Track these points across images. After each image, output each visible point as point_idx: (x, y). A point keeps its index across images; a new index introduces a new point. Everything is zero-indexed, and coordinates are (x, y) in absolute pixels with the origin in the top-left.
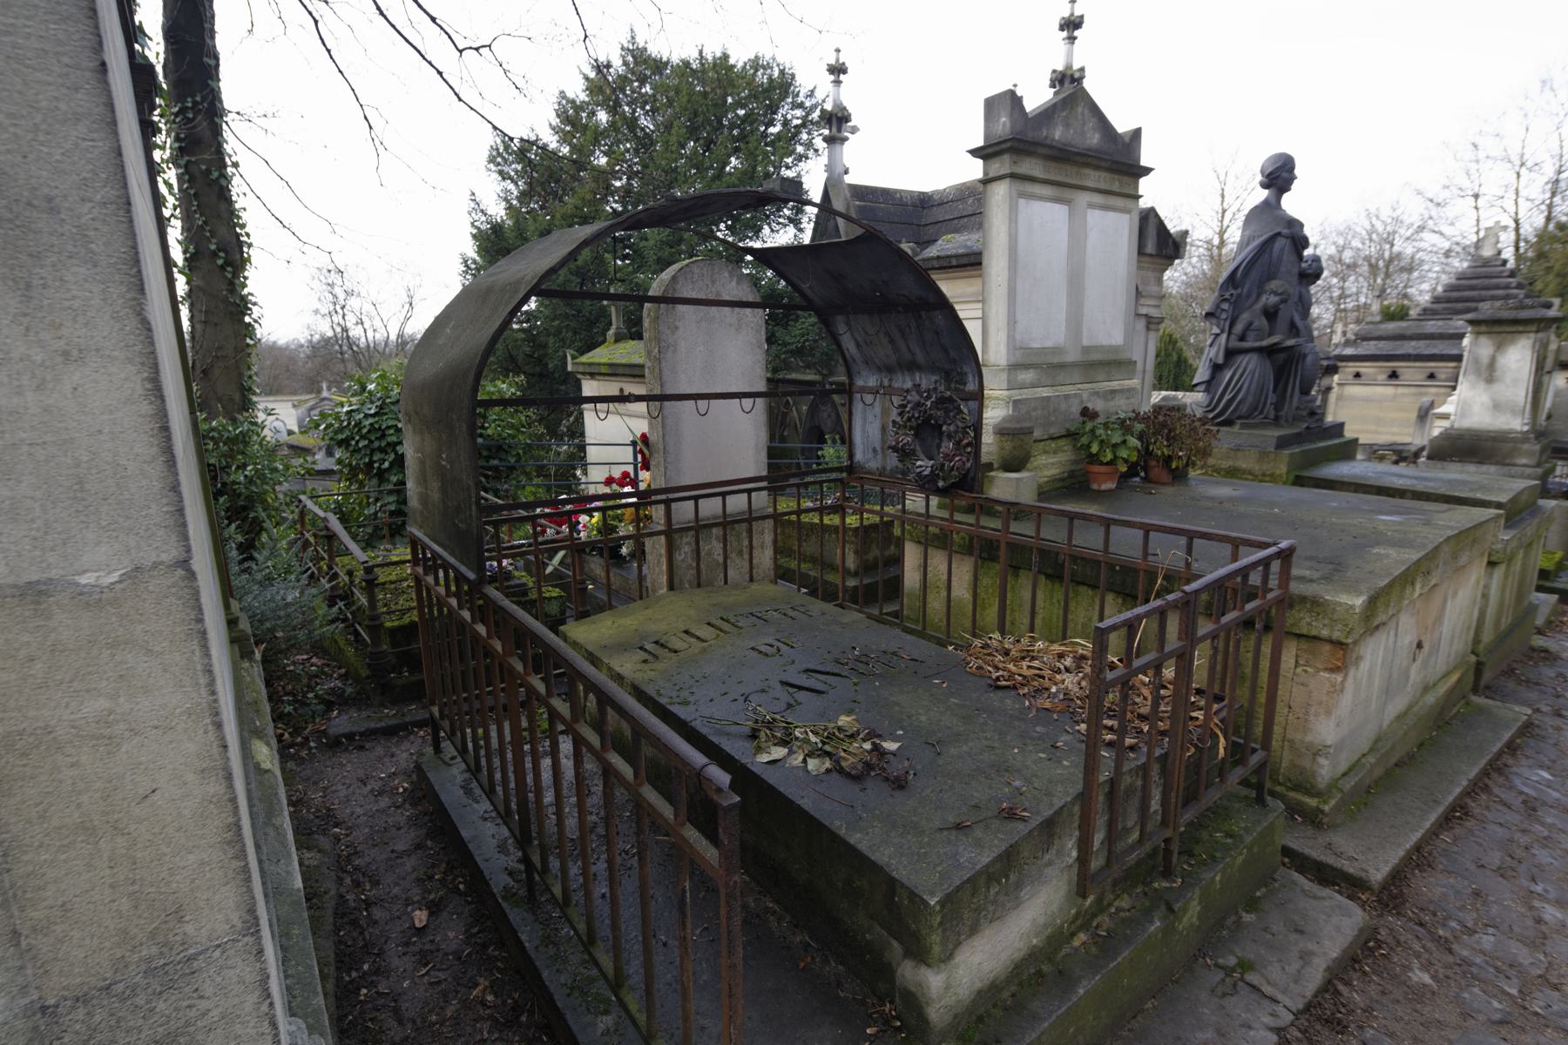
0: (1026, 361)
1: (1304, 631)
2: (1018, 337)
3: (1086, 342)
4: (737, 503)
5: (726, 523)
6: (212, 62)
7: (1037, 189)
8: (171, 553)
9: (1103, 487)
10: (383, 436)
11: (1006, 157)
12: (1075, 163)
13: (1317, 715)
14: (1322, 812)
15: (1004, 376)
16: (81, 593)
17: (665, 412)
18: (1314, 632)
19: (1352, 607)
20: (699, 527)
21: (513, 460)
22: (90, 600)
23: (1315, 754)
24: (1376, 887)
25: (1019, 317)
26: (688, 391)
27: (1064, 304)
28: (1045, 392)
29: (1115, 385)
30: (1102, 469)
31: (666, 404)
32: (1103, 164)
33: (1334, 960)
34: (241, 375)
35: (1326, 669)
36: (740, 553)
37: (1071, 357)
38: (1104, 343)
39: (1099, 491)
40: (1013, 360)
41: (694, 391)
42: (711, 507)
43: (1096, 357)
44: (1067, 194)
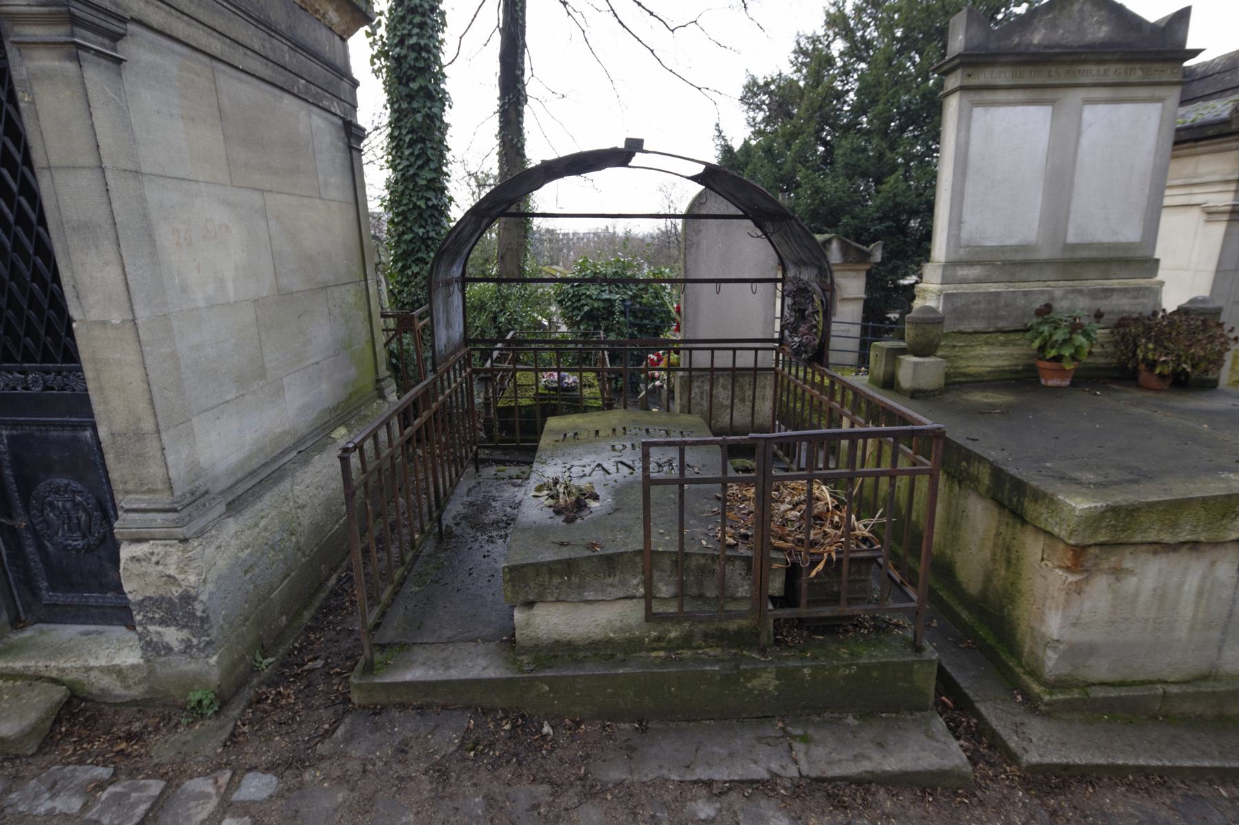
0: (973, 257)
1: (1042, 526)
2: (964, 235)
3: (1071, 238)
4: (745, 359)
5: (735, 373)
6: (519, 73)
7: (1001, 96)
8: (131, 317)
9: (1050, 383)
10: (579, 300)
11: (959, 72)
12: (1064, 63)
13: (1050, 609)
14: (1041, 699)
15: (940, 272)
16: (112, 325)
17: (687, 291)
18: (1049, 529)
19: (1074, 509)
20: (712, 372)
21: (658, 321)
22: (115, 327)
23: (1046, 645)
24: (1024, 765)
25: (967, 217)
26: (707, 277)
27: (1038, 202)
28: (993, 288)
29: (1113, 283)
30: (1047, 365)
31: (723, 285)
32: (1108, 57)
33: (884, 772)
34: (519, 260)
35: (1060, 567)
36: (743, 400)
37: (1043, 255)
38: (1105, 240)
39: (1046, 387)
40: (953, 257)
41: (712, 277)
42: (723, 359)
43: (1079, 254)
44: (1048, 94)
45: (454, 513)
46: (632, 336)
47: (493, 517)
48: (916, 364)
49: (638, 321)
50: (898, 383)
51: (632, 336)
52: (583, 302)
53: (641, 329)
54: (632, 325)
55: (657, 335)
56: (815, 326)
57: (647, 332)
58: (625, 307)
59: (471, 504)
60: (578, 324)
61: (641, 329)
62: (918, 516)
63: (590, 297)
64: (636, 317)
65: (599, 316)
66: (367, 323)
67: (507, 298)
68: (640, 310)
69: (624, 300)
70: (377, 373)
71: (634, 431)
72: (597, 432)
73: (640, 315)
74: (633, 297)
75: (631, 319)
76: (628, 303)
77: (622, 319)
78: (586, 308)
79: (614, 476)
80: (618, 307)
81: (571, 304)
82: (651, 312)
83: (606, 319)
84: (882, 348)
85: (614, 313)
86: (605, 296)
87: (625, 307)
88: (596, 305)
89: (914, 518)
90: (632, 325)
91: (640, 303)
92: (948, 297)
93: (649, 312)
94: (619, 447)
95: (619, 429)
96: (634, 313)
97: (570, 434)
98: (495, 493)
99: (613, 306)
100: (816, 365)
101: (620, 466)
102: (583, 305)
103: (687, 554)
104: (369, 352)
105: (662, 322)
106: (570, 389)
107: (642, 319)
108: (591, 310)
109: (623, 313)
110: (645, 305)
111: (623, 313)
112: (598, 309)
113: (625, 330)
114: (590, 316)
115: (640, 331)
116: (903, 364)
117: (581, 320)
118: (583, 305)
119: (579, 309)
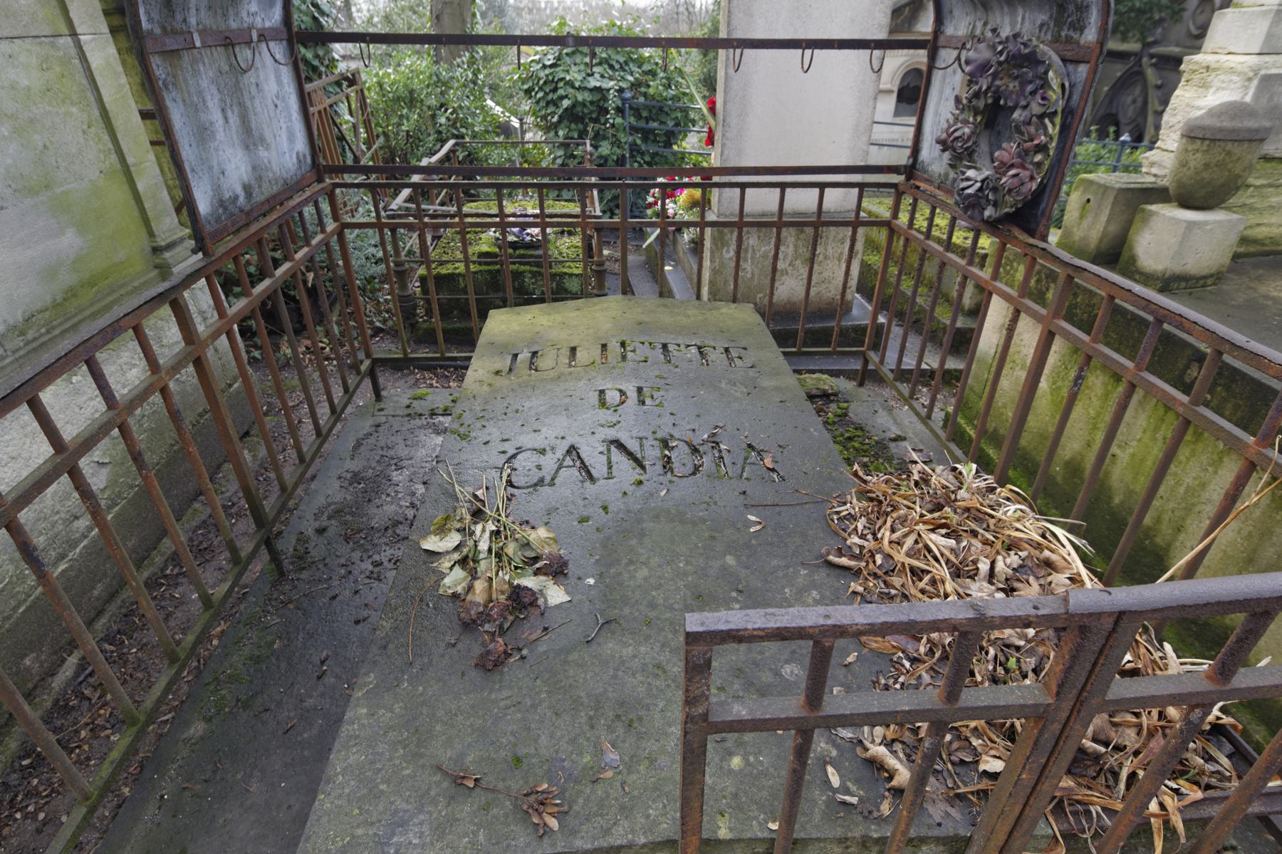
10: (555, 90)
21: (671, 123)
45: (321, 500)
46: (634, 148)
47: (390, 509)
48: (1191, 225)
49: (642, 124)
50: (1133, 259)
51: (634, 148)
52: (561, 92)
53: (647, 135)
54: (634, 130)
55: (668, 145)
56: (1042, 148)
57: (655, 141)
58: (624, 100)
59: (356, 478)
60: (555, 127)
61: (647, 135)
62: (1158, 520)
63: (570, 84)
64: (639, 117)
65: (583, 117)
66: (99, 130)
67: (446, 84)
68: (646, 107)
69: (621, 91)
70: (151, 234)
71: (639, 356)
72: (573, 350)
73: (645, 114)
74: (635, 85)
75: (632, 120)
76: (628, 95)
77: (619, 120)
78: (566, 103)
79: (601, 489)
80: (613, 102)
81: (545, 90)
82: (661, 109)
83: (596, 121)
84: (1105, 188)
85: (607, 112)
86: (593, 83)
87: (624, 100)
88: (580, 98)
89: (1147, 520)
90: (634, 130)
91: (645, 95)
92: (1268, 81)
93: (658, 109)
94: (612, 397)
95: (614, 346)
96: (637, 112)
97: (524, 356)
98: (402, 451)
99: (605, 99)
100: (1017, 232)
101: (616, 455)
102: (562, 98)
103: (795, 842)
104: (118, 194)
105: (677, 125)
106: (531, 246)
107: (647, 120)
108: (574, 106)
109: (619, 110)
110: (653, 97)
111: (619, 110)
112: (583, 104)
113: (623, 138)
114: (572, 115)
115: (645, 139)
116: (1155, 224)
117: (560, 122)
118: (562, 98)
119: (555, 103)
